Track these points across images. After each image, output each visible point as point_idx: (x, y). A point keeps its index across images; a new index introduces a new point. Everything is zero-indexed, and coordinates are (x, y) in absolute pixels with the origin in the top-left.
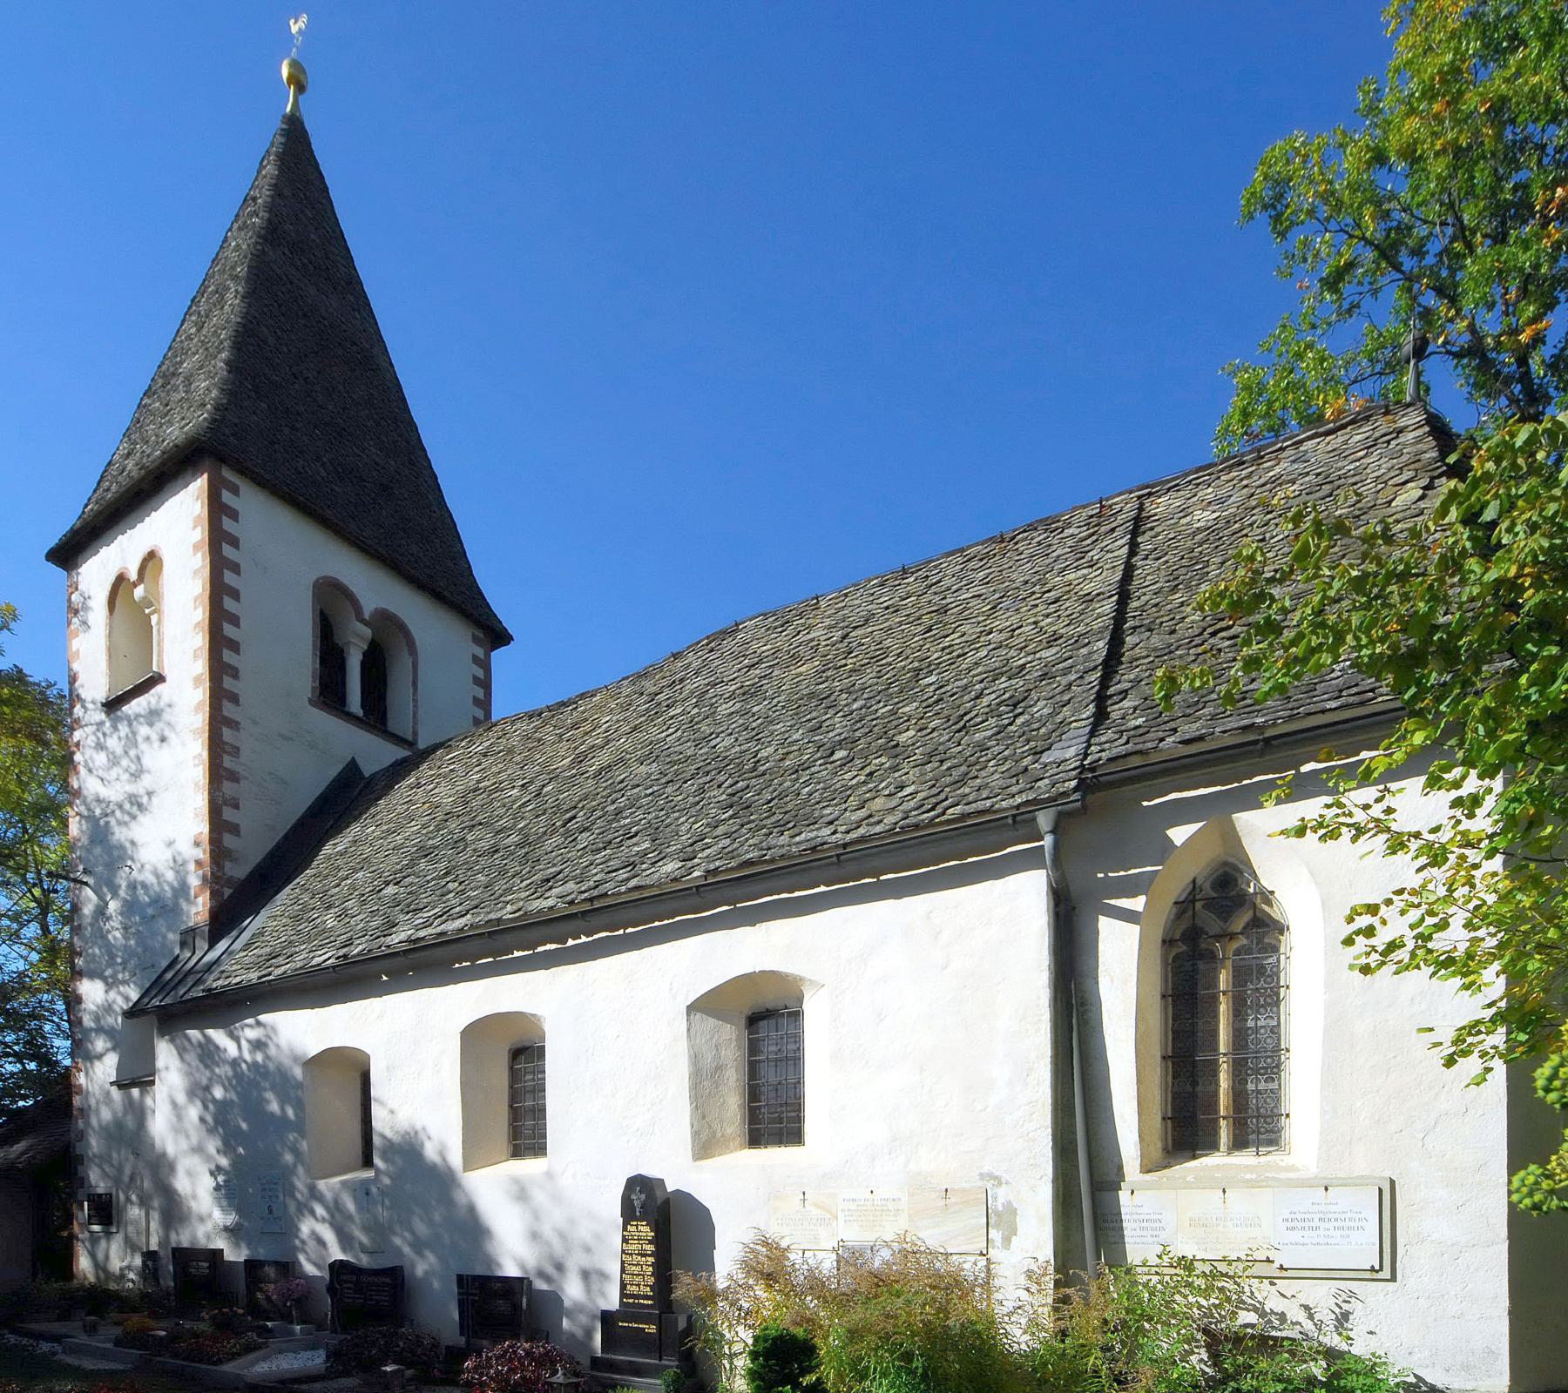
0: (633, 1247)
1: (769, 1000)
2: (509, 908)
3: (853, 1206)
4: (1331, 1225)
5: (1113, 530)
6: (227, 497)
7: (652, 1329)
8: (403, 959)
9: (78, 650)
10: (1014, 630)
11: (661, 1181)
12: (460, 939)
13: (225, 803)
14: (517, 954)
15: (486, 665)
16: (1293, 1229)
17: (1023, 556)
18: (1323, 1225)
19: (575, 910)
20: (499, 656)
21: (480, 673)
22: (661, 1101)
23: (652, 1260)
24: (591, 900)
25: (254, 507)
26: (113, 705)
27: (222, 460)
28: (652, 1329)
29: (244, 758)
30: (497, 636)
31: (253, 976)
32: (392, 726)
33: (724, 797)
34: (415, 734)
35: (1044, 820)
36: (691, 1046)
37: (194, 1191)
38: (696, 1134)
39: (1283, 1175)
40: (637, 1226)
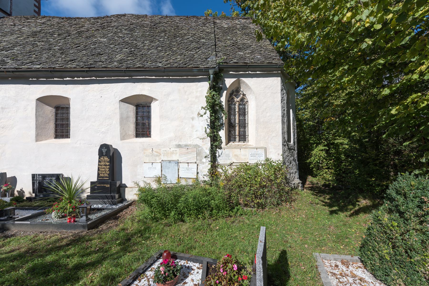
0: (103, 163)
1: (141, 101)
2: (58, 65)
3: (165, 152)
4: (257, 156)
5: (210, 22)
8: (12, 73)
11: (111, 146)
18: (256, 156)
22: (111, 124)
23: (108, 167)
24: (89, 68)
28: (108, 186)
35: (211, 72)
37: (367, 18)
38: (121, 134)
39: (250, 146)
40: (104, 158)
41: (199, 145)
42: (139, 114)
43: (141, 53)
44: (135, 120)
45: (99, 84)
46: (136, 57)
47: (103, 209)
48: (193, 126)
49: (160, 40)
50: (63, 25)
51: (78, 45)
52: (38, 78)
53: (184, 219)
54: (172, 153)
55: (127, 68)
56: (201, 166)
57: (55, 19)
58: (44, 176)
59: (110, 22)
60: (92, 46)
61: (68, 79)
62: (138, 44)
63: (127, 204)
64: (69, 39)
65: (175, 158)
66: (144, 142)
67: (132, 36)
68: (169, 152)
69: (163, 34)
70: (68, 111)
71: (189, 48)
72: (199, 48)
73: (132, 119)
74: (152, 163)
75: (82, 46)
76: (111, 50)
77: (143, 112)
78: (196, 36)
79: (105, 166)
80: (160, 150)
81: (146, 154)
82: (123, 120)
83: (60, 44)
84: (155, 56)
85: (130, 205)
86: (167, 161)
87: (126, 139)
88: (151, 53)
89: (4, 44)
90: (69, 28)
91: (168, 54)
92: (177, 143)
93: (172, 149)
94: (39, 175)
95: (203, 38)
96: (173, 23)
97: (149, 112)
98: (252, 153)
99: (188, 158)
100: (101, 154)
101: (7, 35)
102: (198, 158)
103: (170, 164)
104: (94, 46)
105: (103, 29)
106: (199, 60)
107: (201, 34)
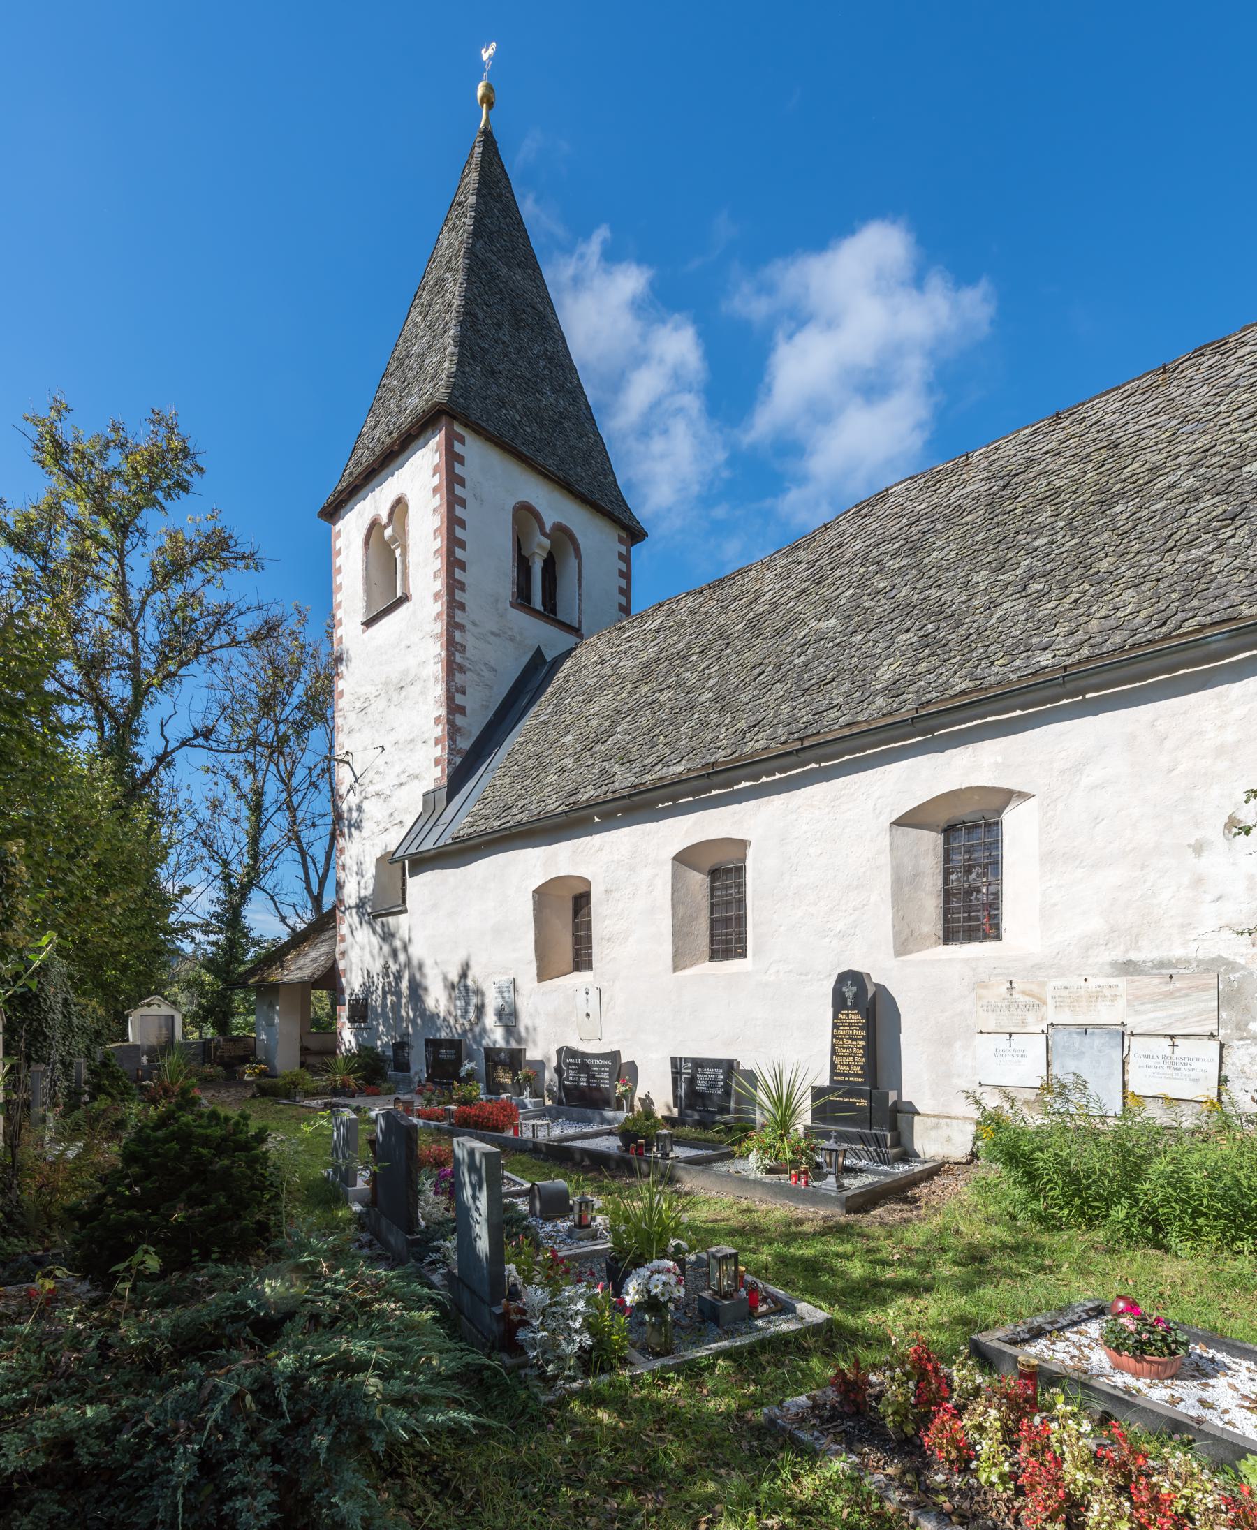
0: (845, 1032)
1: (964, 812)
3: (1065, 993)
6: (457, 447)
7: (863, 1103)
10: (1207, 450)
12: (679, 781)
13: (457, 691)
14: (714, 793)
15: (625, 558)
17: (1194, 382)
19: (787, 748)
20: (640, 552)
21: (623, 567)
24: (802, 739)
25: (474, 449)
27: (453, 417)
29: (468, 654)
30: (634, 533)
32: (561, 616)
33: (915, 639)
34: (580, 622)
36: (893, 858)
38: (896, 935)
41: (1231, 958)
42: (955, 857)
43: (962, 631)
44: (940, 881)
45: (828, 781)
46: (946, 656)
47: (861, 1171)
48: (1198, 881)
49: (1036, 544)
50: (707, 613)
51: (758, 670)
52: (674, 798)
53: (1165, 1241)
54: (1097, 996)
56: (1242, 1051)
57: (683, 603)
58: (699, 1064)
59: (840, 546)
60: (796, 661)
61: (744, 784)
62: (948, 597)
63: (918, 1168)
64: (729, 655)
65: (1107, 1014)
66: (977, 959)
67: (920, 571)
68: (1082, 992)
69: (1045, 516)
70: (740, 877)
71: (1176, 537)
72: (1233, 519)
73: (932, 881)
74: (1011, 1034)
75: (770, 668)
76: (858, 653)
77: (970, 850)
78: (1216, 454)
79: (853, 1040)
80: (1042, 984)
81: (984, 1002)
82: (902, 887)
83: (711, 683)
84: (1020, 626)
85: (931, 1174)
86: (1073, 1029)
87: (910, 952)
88: (1003, 619)
89: (594, 723)
90: (722, 619)
91: (1076, 601)
92: (1118, 955)
93: (1093, 983)
96: (1091, 436)
97: (995, 845)
99: (1170, 1016)
100: (839, 1003)
101: (593, 696)
102: (1224, 1015)
103: (1087, 1040)
104: (802, 658)
105: (819, 583)
106: (1235, 578)
107: (1245, 437)
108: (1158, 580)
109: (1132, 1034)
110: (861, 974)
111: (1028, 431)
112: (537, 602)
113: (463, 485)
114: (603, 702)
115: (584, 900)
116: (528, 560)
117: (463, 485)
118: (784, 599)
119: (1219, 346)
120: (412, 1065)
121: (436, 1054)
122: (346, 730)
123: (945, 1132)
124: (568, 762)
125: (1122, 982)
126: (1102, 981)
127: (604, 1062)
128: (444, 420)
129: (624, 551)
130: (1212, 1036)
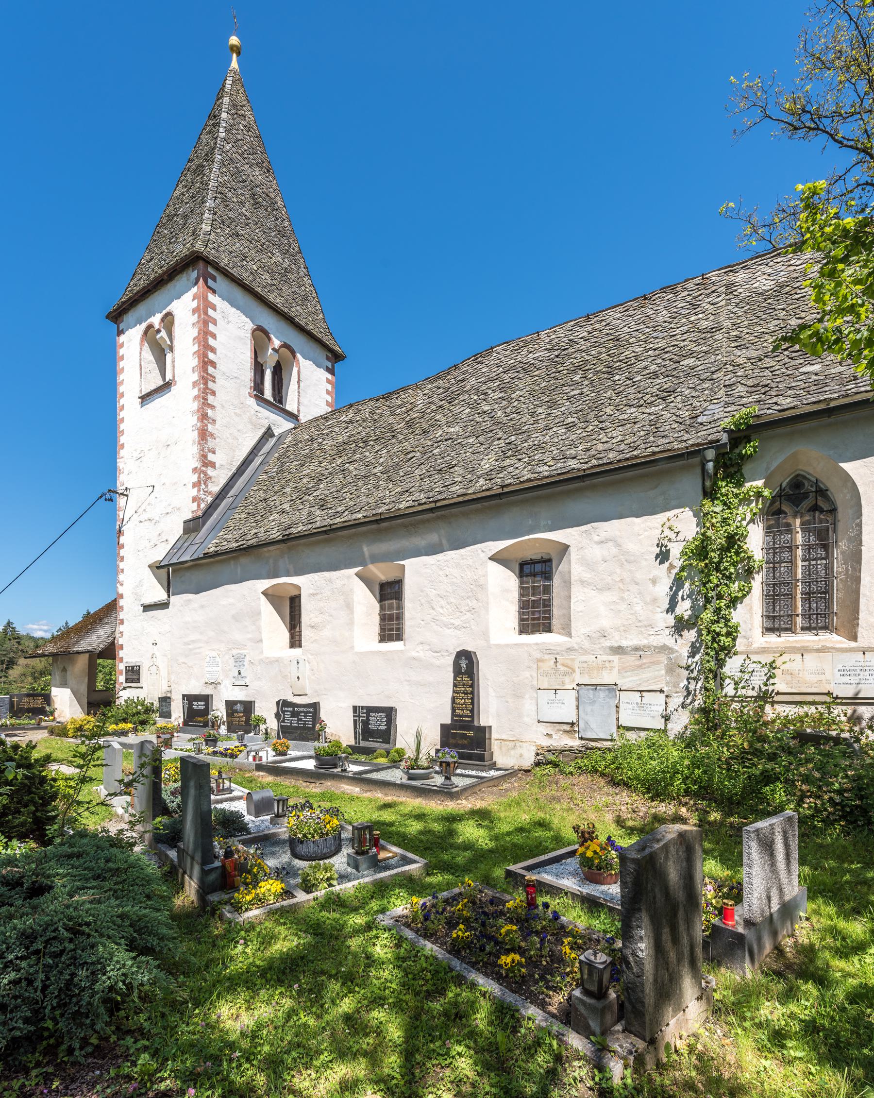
3: (585, 665)
4: (867, 673)
9: (123, 368)
16: (844, 675)
18: (862, 673)
24: (435, 502)
26: (145, 398)
31: (235, 545)
34: (299, 411)
54: (601, 667)
55: (503, 487)
58: (370, 710)
60: (434, 452)
63: (493, 773)
65: (608, 678)
74: (556, 690)
81: (541, 670)
90: (391, 420)
94: (363, 708)
95: (691, 354)
98: (846, 665)
101: (305, 463)
105: (450, 403)
108: (635, 423)
109: (620, 690)
110: (470, 652)
111: (572, 323)
112: (268, 394)
113: (215, 310)
114: (311, 468)
115: (297, 600)
116: (262, 366)
117: (215, 310)
118: (428, 411)
119: (671, 288)
120: (173, 713)
121: (190, 704)
122: (126, 472)
123: (519, 751)
124: (286, 506)
125: (616, 658)
126: (605, 657)
127: (308, 710)
128: (201, 264)
129: (330, 366)
130: (662, 691)
